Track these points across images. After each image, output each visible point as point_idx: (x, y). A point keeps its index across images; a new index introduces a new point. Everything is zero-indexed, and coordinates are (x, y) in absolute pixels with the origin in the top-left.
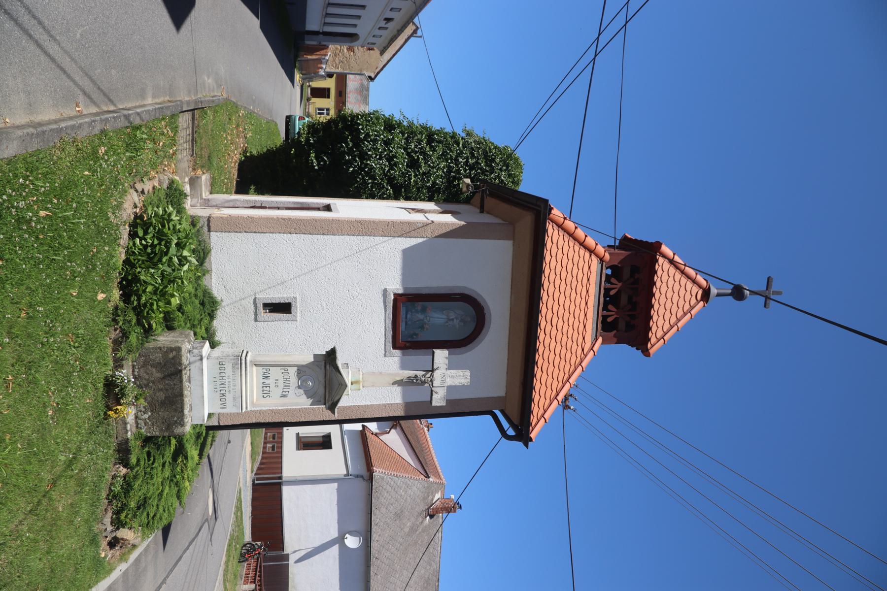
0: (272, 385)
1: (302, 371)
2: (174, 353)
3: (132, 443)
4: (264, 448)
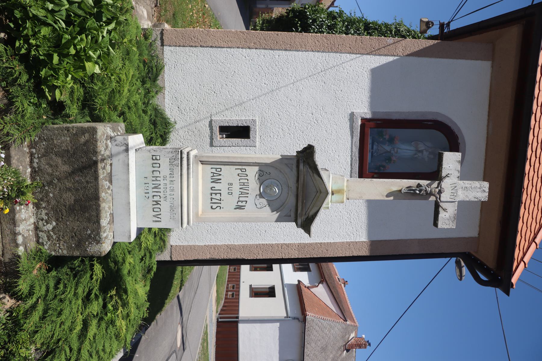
0: (224, 192)
1: (266, 172)
2: (87, 135)
3: (24, 263)
4: (226, 295)
